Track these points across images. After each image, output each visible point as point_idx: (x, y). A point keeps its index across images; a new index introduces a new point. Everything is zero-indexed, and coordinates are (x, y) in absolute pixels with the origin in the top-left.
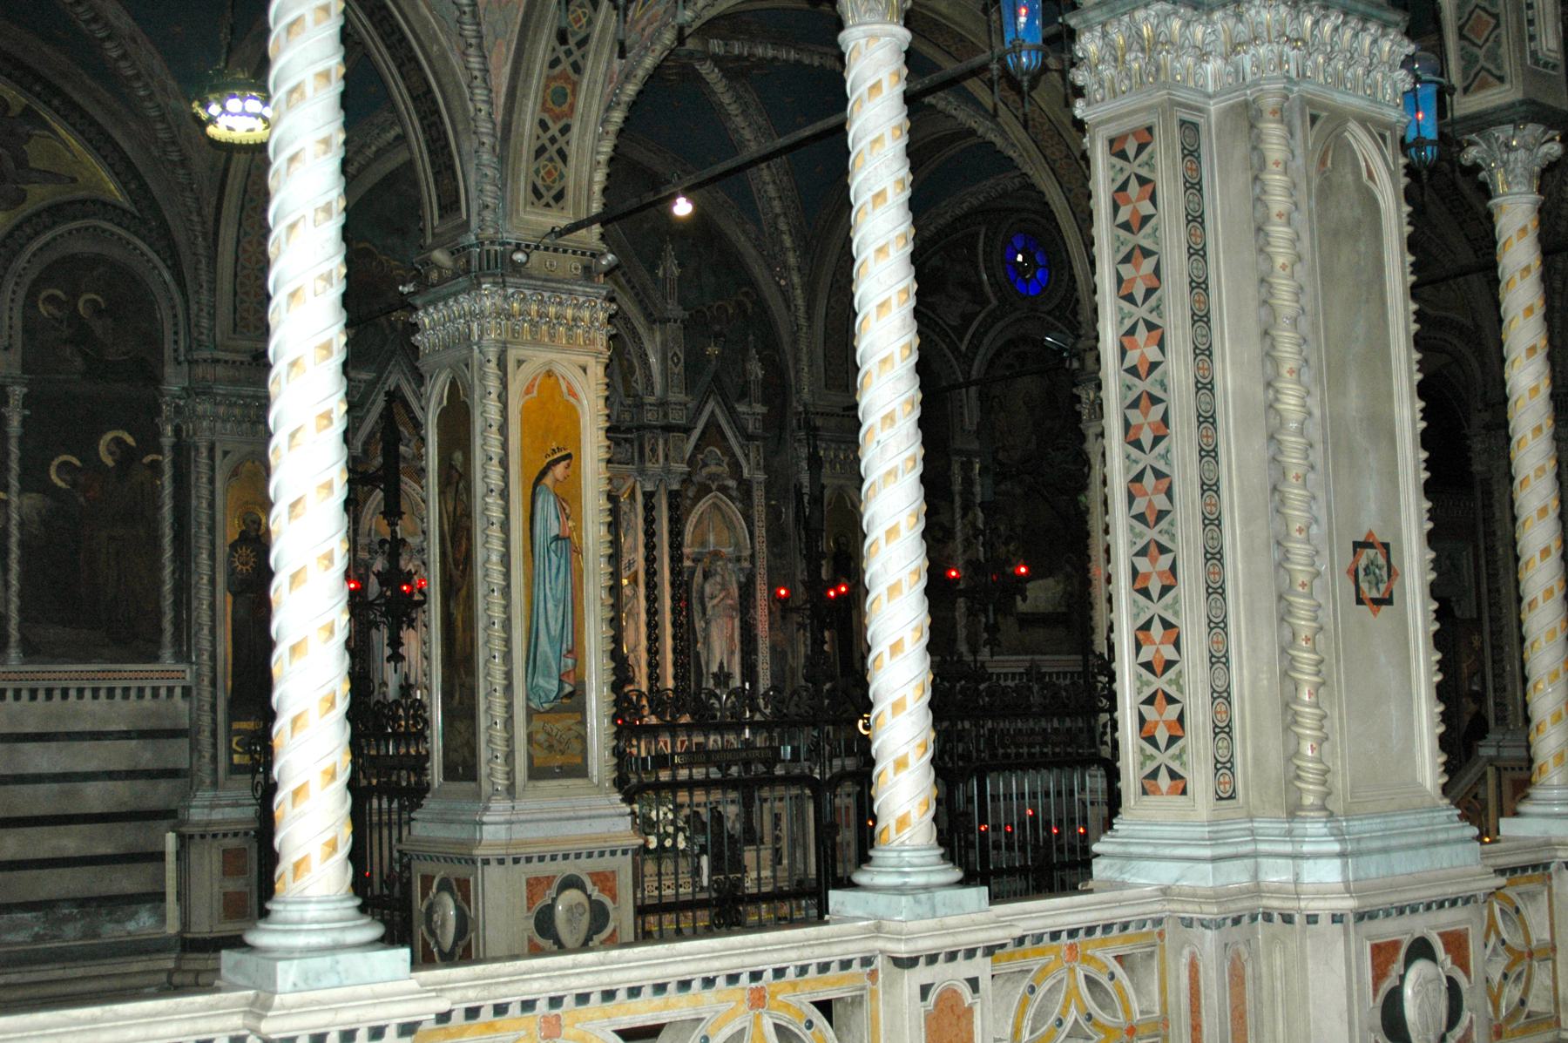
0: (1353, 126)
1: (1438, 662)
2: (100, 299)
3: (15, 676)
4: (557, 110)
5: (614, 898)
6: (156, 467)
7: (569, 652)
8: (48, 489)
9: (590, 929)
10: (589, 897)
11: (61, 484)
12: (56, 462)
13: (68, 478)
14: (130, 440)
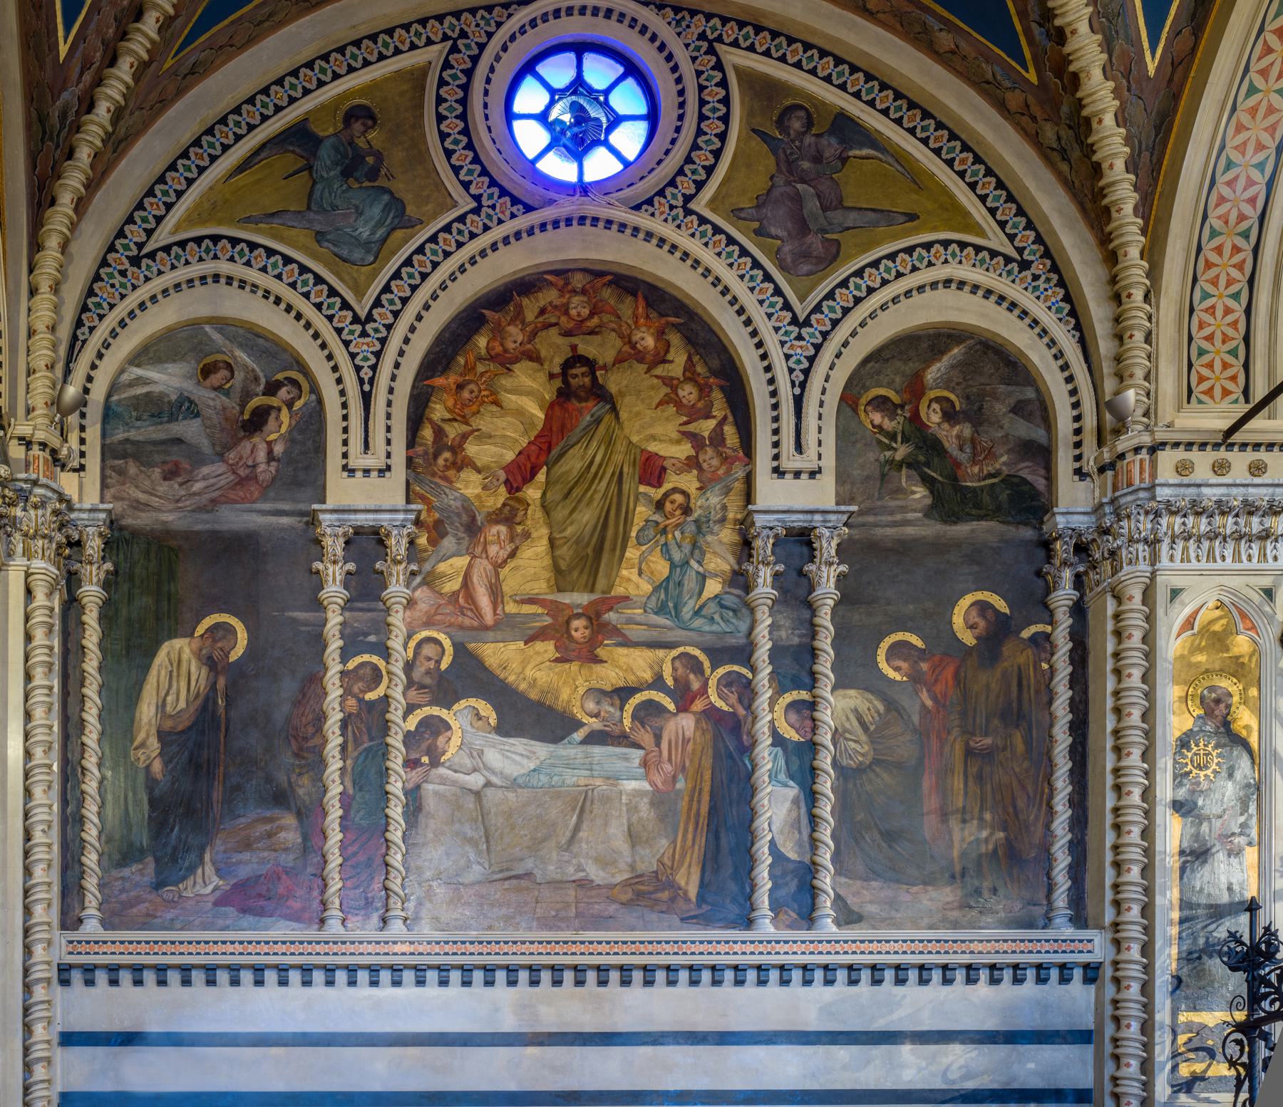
0: (207, 328)
3: (607, 948)
6: (1043, 643)
11: (892, 674)
13: (904, 665)
14: (1001, 605)
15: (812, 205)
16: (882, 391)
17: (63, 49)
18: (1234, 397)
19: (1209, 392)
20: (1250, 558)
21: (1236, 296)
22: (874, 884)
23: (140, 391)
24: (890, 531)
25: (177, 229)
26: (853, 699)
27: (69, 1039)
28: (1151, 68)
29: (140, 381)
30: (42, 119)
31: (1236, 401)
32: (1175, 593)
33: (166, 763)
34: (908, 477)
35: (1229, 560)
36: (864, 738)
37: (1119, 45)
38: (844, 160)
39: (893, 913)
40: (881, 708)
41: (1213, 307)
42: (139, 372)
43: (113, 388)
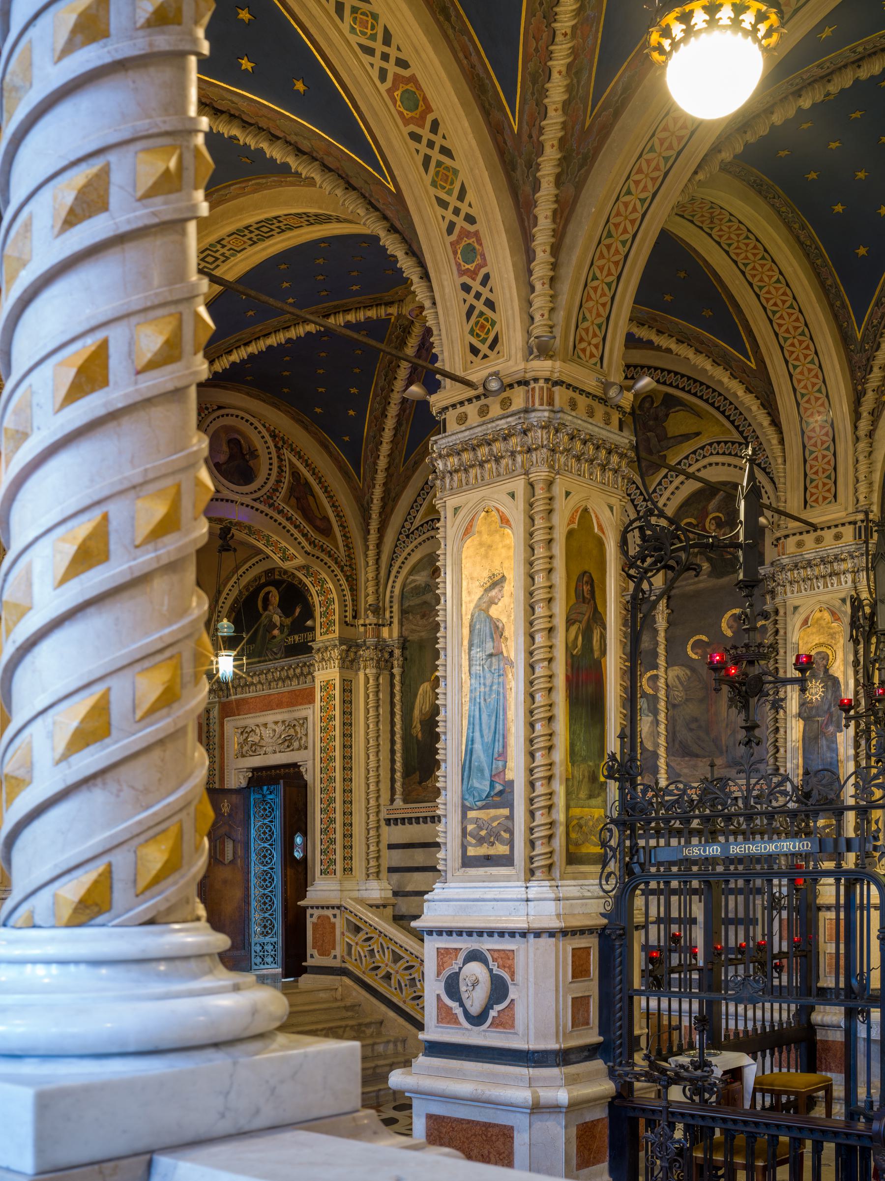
1: (438, 643)
2: (721, 515)
4: (471, 267)
5: (512, 975)
7: (500, 755)
8: (688, 663)
9: (490, 998)
10: (491, 971)
11: (694, 656)
12: (692, 641)
13: (699, 651)
15: (654, 441)
16: (688, 520)
17: (361, 485)
18: (829, 500)
19: (816, 501)
20: (832, 585)
21: (827, 449)
22: (687, 759)
23: (413, 585)
24: (692, 587)
25: (420, 520)
26: (676, 671)
27: (391, 847)
28: (753, 366)
29: (414, 581)
30: (362, 506)
31: (830, 502)
32: (796, 608)
33: (422, 734)
34: (701, 559)
35: (821, 588)
36: (681, 689)
37: (733, 364)
38: (667, 415)
39: (695, 772)
40: (688, 673)
41: (817, 457)
42: (412, 578)
43: (404, 586)
